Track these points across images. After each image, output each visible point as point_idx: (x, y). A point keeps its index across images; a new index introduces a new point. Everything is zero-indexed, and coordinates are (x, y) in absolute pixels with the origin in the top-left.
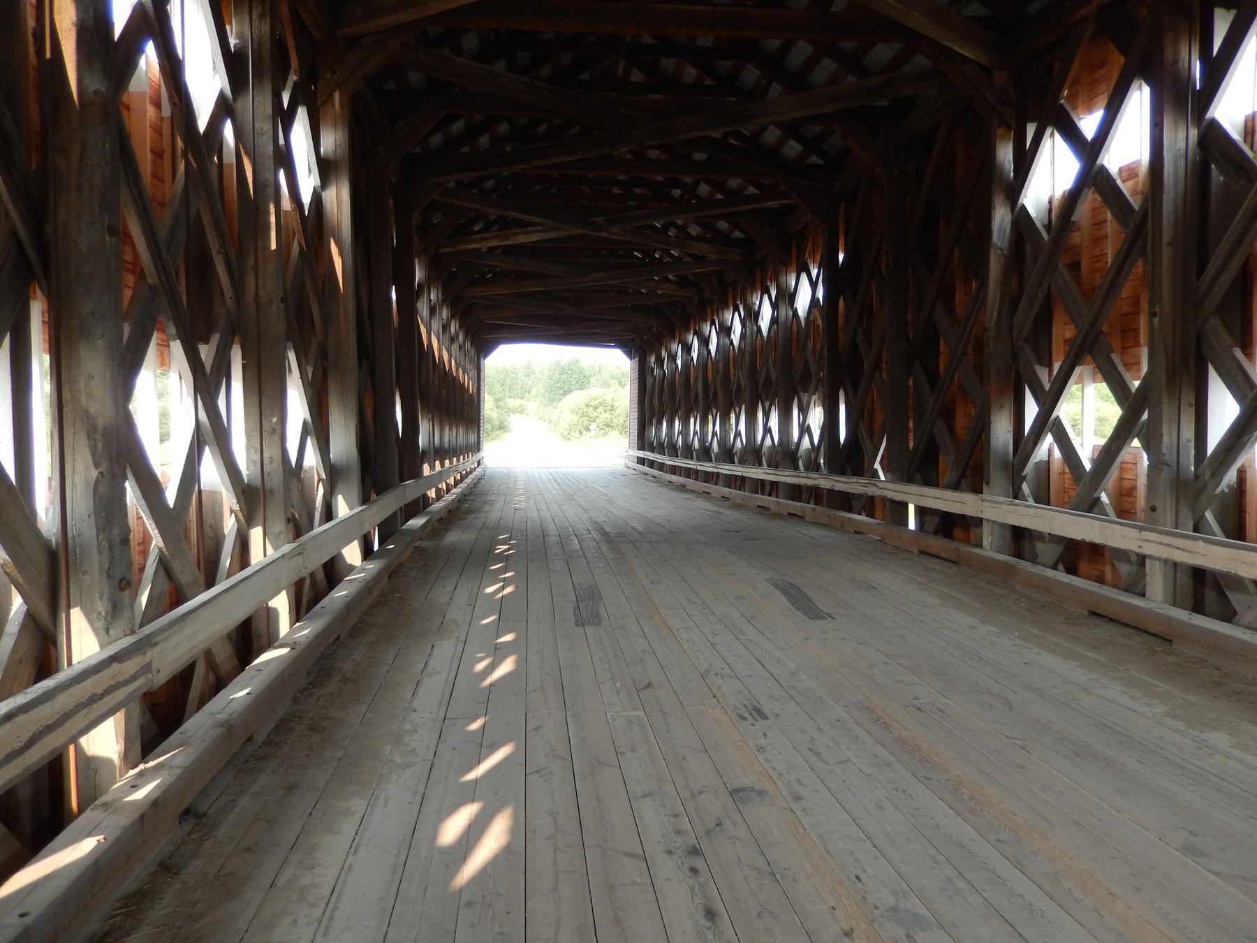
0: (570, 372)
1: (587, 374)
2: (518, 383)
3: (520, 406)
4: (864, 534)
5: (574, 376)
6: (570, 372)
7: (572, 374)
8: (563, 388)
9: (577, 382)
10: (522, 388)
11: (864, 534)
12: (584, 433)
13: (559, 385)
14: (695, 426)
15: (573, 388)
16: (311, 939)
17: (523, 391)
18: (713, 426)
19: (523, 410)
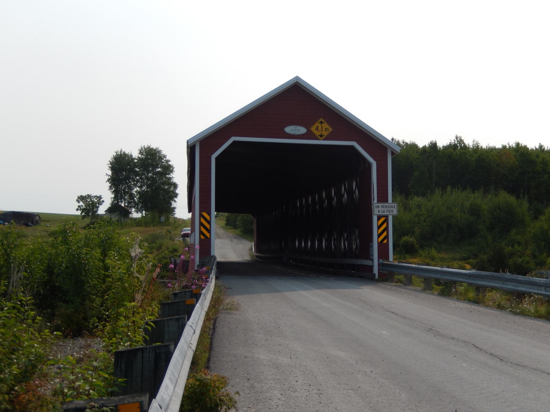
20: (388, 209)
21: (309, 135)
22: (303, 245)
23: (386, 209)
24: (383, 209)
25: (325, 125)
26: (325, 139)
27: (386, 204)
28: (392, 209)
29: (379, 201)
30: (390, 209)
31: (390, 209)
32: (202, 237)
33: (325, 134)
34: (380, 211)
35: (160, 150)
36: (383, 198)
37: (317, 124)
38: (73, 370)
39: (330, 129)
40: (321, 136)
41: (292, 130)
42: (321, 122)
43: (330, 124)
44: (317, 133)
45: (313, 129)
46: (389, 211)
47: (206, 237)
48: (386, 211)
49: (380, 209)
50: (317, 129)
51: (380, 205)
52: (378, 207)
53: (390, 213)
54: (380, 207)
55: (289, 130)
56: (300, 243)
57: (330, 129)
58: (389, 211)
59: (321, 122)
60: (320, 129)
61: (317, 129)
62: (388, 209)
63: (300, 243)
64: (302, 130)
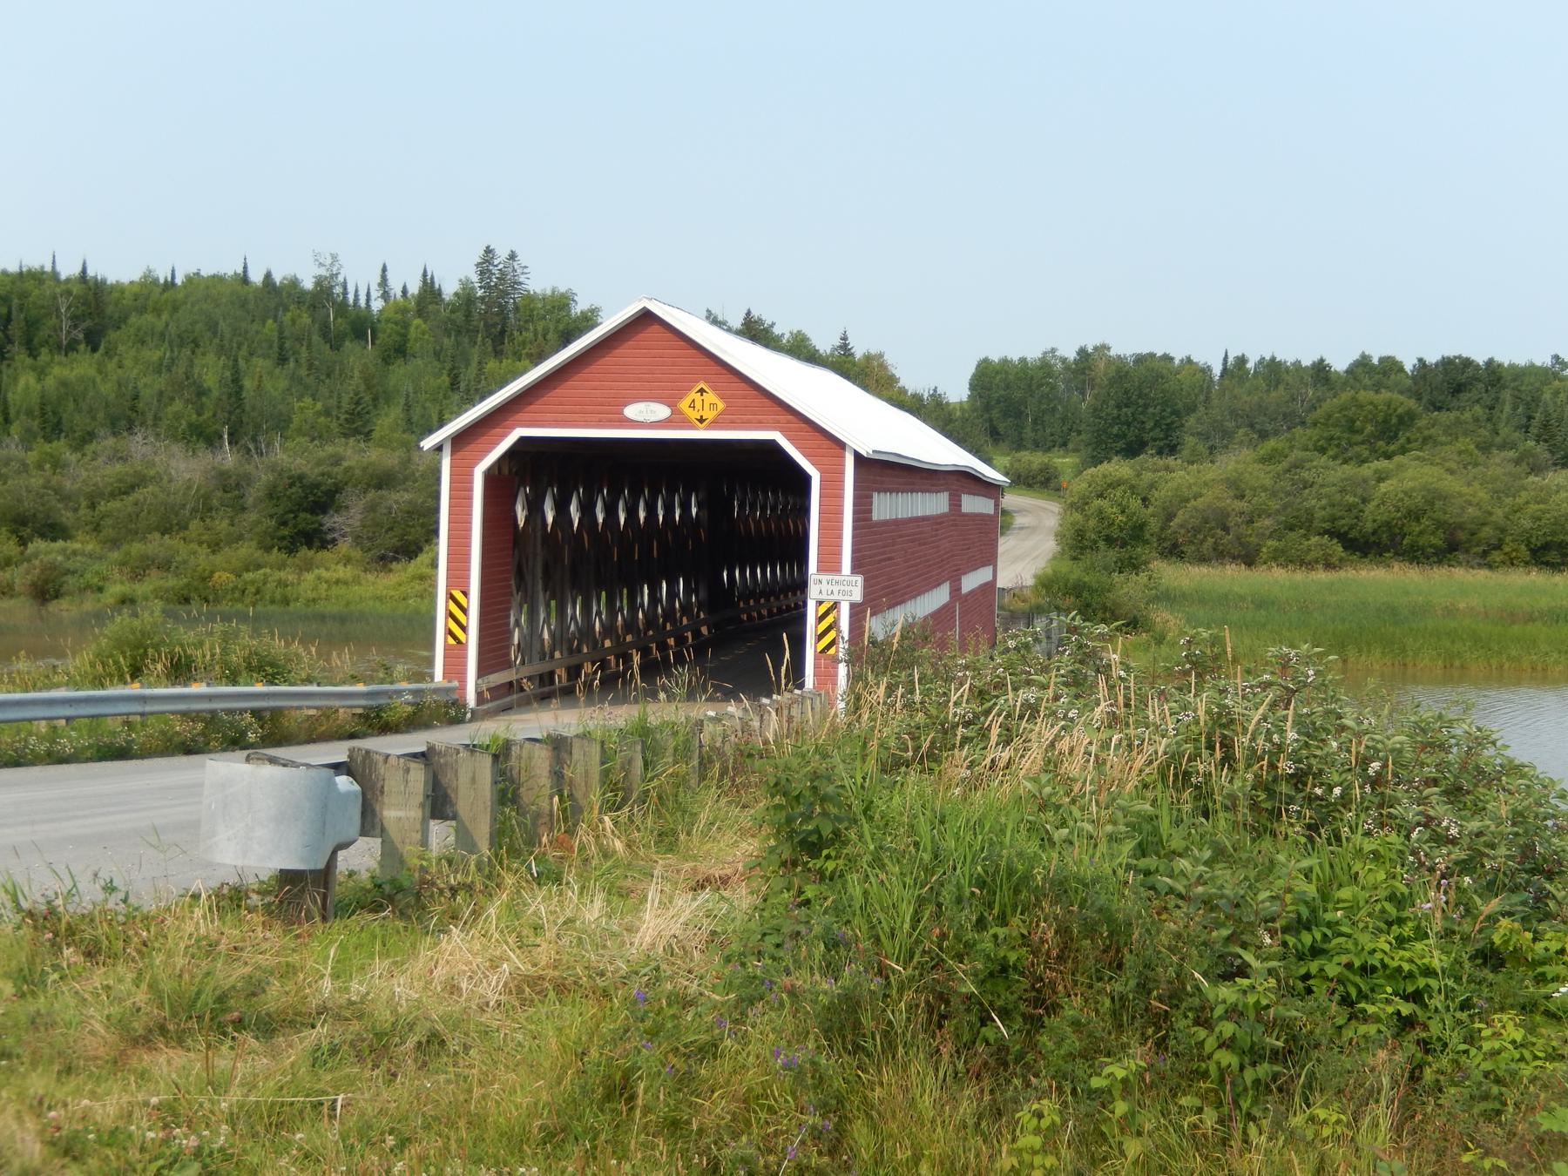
0: (1141, 402)
1: (1180, 405)
2: (1054, 409)
3: (1041, 471)
4: (384, 269)
5: (1151, 410)
6: (1141, 402)
7: (1146, 406)
8: (1125, 436)
9: (1157, 424)
10: (1064, 420)
11: (384, 269)
12: (124, 569)
13: (1115, 430)
14: (600, 606)
15: (1146, 437)
16: (892, 380)
17: (1065, 429)
18: (600, 606)
19: (1048, 480)
20: (842, 588)
21: (676, 420)
22: (642, 515)
23: (836, 589)
24: (830, 588)
25: (710, 397)
26: (708, 428)
27: (837, 578)
28: (850, 588)
29: (821, 569)
30: (846, 588)
31: (846, 588)
32: (451, 641)
33: (710, 415)
34: (824, 592)
35: (695, 700)
36: (830, 564)
37: (693, 395)
38: (997, 505)
39: (721, 406)
40: (701, 420)
41: (641, 412)
42: (702, 391)
43: (722, 398)
44: (693, 415)
45: (684, 405)
46: (844, 593)
47: (459, 642)
48: (836, 592)
49: (824, 587)
50: (692, 406)
51: (825, 577)
52: (820, 582)
53: (846, 598)
54: (824, 582)
55: (632, 411)
56: (535, 508)
57: (721, 406)
58: (844, 593)
59: (702, 391)
60: (698, 405)
61: (692, 406)
62: (842, 588)
63: (535, 508)
64: (661, 411)
